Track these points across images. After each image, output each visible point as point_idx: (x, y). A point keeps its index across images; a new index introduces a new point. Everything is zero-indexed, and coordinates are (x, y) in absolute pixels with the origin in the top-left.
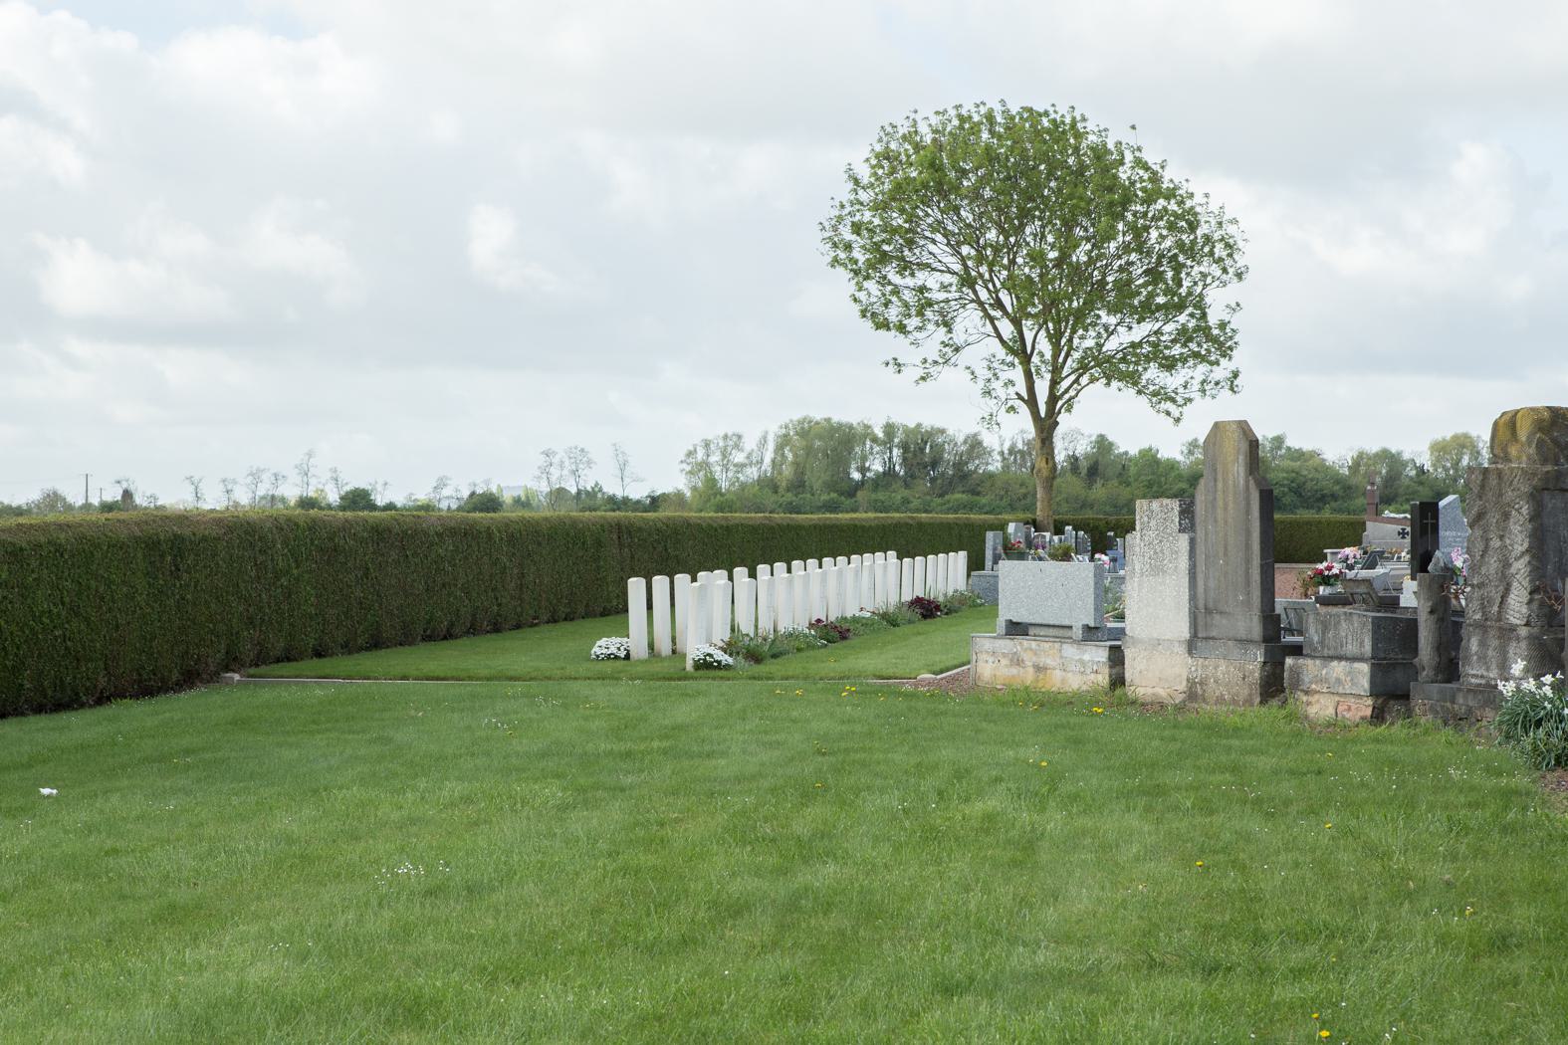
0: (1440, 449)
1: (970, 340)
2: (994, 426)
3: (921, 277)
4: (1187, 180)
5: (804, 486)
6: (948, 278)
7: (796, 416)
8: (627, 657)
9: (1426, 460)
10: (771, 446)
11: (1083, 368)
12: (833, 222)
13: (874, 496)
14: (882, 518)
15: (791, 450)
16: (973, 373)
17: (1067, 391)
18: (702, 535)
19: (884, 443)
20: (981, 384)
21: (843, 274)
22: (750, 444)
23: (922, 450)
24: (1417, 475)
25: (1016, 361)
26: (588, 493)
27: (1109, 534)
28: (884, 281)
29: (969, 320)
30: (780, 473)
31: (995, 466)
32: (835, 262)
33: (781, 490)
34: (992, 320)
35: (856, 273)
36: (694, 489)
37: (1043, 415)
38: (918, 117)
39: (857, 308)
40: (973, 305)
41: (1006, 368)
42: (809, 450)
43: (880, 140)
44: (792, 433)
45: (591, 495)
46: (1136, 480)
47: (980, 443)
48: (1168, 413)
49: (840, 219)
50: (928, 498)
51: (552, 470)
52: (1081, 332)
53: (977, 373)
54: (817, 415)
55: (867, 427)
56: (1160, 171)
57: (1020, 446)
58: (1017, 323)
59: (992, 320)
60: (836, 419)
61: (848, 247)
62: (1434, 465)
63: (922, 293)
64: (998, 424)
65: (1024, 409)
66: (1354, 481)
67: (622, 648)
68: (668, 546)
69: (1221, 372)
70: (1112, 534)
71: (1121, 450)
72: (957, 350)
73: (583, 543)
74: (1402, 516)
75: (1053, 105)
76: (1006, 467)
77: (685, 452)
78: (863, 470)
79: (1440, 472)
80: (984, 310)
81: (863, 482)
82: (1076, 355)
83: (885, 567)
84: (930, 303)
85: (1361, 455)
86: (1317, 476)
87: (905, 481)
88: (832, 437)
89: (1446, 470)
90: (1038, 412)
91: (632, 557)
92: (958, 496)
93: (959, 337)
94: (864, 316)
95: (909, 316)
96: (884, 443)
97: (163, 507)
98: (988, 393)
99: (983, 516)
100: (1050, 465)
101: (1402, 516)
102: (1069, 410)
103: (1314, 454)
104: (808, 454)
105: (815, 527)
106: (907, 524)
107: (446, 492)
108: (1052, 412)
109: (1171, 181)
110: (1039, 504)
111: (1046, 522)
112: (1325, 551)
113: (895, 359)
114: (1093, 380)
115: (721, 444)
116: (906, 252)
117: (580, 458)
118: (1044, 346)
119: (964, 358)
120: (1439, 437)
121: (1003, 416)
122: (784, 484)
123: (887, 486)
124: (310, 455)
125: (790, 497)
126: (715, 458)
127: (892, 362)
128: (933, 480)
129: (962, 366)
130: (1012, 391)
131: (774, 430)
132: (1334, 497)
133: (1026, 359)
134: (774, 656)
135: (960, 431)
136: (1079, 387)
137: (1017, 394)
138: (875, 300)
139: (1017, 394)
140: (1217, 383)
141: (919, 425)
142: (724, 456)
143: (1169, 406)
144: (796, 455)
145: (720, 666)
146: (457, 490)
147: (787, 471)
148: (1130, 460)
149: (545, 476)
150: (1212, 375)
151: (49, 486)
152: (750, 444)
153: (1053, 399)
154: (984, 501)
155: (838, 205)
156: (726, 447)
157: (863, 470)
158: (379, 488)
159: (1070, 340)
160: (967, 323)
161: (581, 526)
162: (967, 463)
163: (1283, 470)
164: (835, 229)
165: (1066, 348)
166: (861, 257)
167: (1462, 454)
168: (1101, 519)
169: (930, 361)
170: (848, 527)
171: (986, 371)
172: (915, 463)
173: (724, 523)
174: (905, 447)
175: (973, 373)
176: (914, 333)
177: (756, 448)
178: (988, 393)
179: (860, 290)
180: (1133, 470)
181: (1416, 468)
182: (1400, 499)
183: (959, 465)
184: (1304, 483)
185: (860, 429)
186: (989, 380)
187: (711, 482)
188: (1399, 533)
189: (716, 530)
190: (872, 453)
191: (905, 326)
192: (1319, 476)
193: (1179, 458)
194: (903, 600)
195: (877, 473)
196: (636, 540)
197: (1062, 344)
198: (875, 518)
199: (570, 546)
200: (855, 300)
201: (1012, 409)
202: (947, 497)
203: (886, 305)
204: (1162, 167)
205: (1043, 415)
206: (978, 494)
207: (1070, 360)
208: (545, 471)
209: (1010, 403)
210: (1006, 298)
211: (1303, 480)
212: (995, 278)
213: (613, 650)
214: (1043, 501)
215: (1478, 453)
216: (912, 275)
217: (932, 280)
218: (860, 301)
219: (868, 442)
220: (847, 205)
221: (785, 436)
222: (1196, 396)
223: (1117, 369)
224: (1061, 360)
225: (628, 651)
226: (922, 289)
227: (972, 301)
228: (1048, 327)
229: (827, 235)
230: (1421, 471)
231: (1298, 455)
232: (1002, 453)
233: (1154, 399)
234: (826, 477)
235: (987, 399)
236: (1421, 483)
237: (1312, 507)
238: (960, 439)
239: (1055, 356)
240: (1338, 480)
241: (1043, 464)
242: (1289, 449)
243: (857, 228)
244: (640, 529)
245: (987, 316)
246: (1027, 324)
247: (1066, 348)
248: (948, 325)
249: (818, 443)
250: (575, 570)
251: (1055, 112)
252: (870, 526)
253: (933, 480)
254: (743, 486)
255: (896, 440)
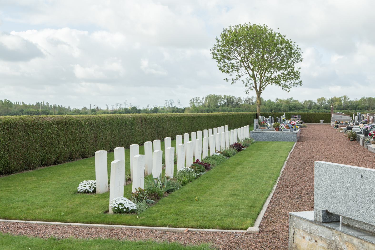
0: (319, 100)
1: (243, 74)
2: (248, 93)
3: (232, 61)
4: (290, 39)
5: (210, 106)
6: (238, 61)
7: (209, 94)
8: (94, 191)
9: (316, 102)
10: (204, 99)
11: (267, 81)
12: (213, 49)
13: (222, 108)
14: (224, 114)
15: (208, 100)
16: (243, 81)
17: (263, 86)
18: (171, 120)
19: (224, 99)
20: (245, 84)
21: (215, 60)
22: (201, 99)
23: (230, 100)
24: (315, 104)
25: (253, 79)
26: (173, 107)
27: (277, 117)
28: (224, 62)
29: (242, 70)
30: (206, 104)
31: (243, 103)
32: (214, 58)
33: (206, 107)
34: (247, 70)
35: (218, 60)
36: (191, 107)
37: (258, 91)
38: (232, 26)
39: (218, 68)
40: (243, 67)
41: (251, 80)
42: (211, 100)
43: (223, 31)
44: (208, 97)
45: (174, 108)
46: (267, 105)
47: (240, 99)
48: (286, 90)
49: (215, 48)
50: (231, 108)
51: (167, 103)
52: (267, 73)
53: (244, 81)
54: (213, 94)
55: (221, 96)
56: (284, 37)
57: (247, 99)
58: (253, 70)
59: (247, 70)
60: (215, 95)
61: (216, 55)
62: (318, 103)
63: (232, 64)
64: (249, 93)
65: (254, 89)
66: (304, 106)
67: (92, 187)
68: (160, 123)
69: (298, 81)
70: (278, 117)
71: (264, 100)
72: (240, 77)
73: (126, 124)
74: (341, 113)
75: (260, 24)
76: (245, 103)
77: (190, 100)
78: (220, 103)
79: (319, 104)
80: (246, 68)
81: (220, 106)
82: (265, 78)
83: (225, 134)
84: (234, 66)
85: (305, 101)
86: (298, 105)
87: (227, 105)
88: (215, 98)
89: (320, 104)
90: (257, 90)
91: (146, 127)
92: (236, 108)
93: (240, 74)
94: (220, 69)
95: (229, 69)
96: (224, 99)
97: (351, 102)
98: (246, 86)
99: (246, 113)
100: (260, 101)
101: (341, 113)
102: (264, 90)
103: (298, 101)
104: (211, 101)
105: (206, 116)
106: (229, 115)
107: (149, 107)
108: (260, 90)
109: (287, 39)
110: (257, 110)
111: (259, 114)
112: (320, 120)
113: (226, 79)
114: (269, 83)
115: (196, 99)
116: (229, 55)
117: (172, 101)
118: (259, 76)
119: (241, 78)
120: (319, 98)
121: (250, 91)
122: (207, 106)
123: (224, 106)
124: (126, 101)
125: (207, 108)
126: (195, 101)
127: (226, 79)
128: (232, 105)
129: (241, 80)
130: (252, 85)
131: (205, 97)
132: (301, 108)
133: (255, 78)
134: (168, 192)
135: (237, 97)
136: (266, 85)
137: (253, 86)
138: (222, 66)
139: (253, 86)
140: (297, 84)
141: (230, 96)
142: (196, 101)
143: (287, 89)
144: (209, 101)
145: (128, 211)
146: (151, 107)
147: (207, 104)
148: (266, 102)
149: (166, 104)
150: (296, 82)
151: (84, 106)
152: (201, 99)
153: (260, 87)
154: (241, 109)
155: (214, 45)
156: (197, 99)
157: (220, 103)
158: (138, 106)
159: (264, 75)
160: (242, 71)
161: (125, 118)
162: (238, 102)
163: (292, 104)
164: (214, 50)
165: (263, 76)
166: (219, 57)
167: (323, 101)
168: (270, 113)
169: (234, 79)
170: (215, 116)
171: (246, 81)
172: (229, 102)
173: (179, 116)
174: (227, 99)
175: (243, 81)
176: (230, 73)
177: (202, 100)
178: (246, 86)
179: (219, 64)
180: (267, 104)
181: (315, 103)
182: (312, 109)
183: (237, 103)
184: (296, 106)
185: (220, 97)
186: (247, 83)
187: (194, 105)
188: (340, 117)
189: (176, 118)
190: (222, 101)
191: (229, 71)
192: (298, 105)
193: (275, 101)
194: (231, 144)
195: (223, 104)
196: (148, 122)
197: (263, 75)
198: (222, 114)
199: (120, 125)
200: (218, 66)
201: (252, 89)
202: (235, 108)
203: (224, 67)
204: (285, 37)
205: (258, 91)
206: (240, 108)
207: (264, 79)
208: (166, 104)
209: (251, 88)
210: (250, 65)
211: (296, 105)
212: (248, 61)
213: (87, 188)
214: (258, 109)
215: (325, 101)
216: (230, 60)
217: (234, 62)
218: (219, 66)
219: (221, 99)
220: (216, 45)
221: (207, 97)
222: (293, 86)
223: (276, 80)
224: (262, 79)
225: (95, 188)
226: (232, 64)
227: (243, 66)
228: (259, 72)
229: (212, 52)
230: (316, 104)
231: (295, 101)
232: (244, 101)
233: (283, 87)
234: (214, 105)
235: (246, 87)
236: (316, 106)
237: (297, 110)
238: (237, 98)
239: (261, 78)
240: (302, 105)
241: (258, 101)
242: (293, 100)
243: (218, 51)
244: (149, 119)
245: (246, 69)
246: (255, 71)
247: (263, 76)
248: (238, 71)
249: (212, 99)
250: (122, 133)
251: (260, 25)
252: (221, 116)
253: (232, 105)
254: (200, 106)
255: (226, 98)
